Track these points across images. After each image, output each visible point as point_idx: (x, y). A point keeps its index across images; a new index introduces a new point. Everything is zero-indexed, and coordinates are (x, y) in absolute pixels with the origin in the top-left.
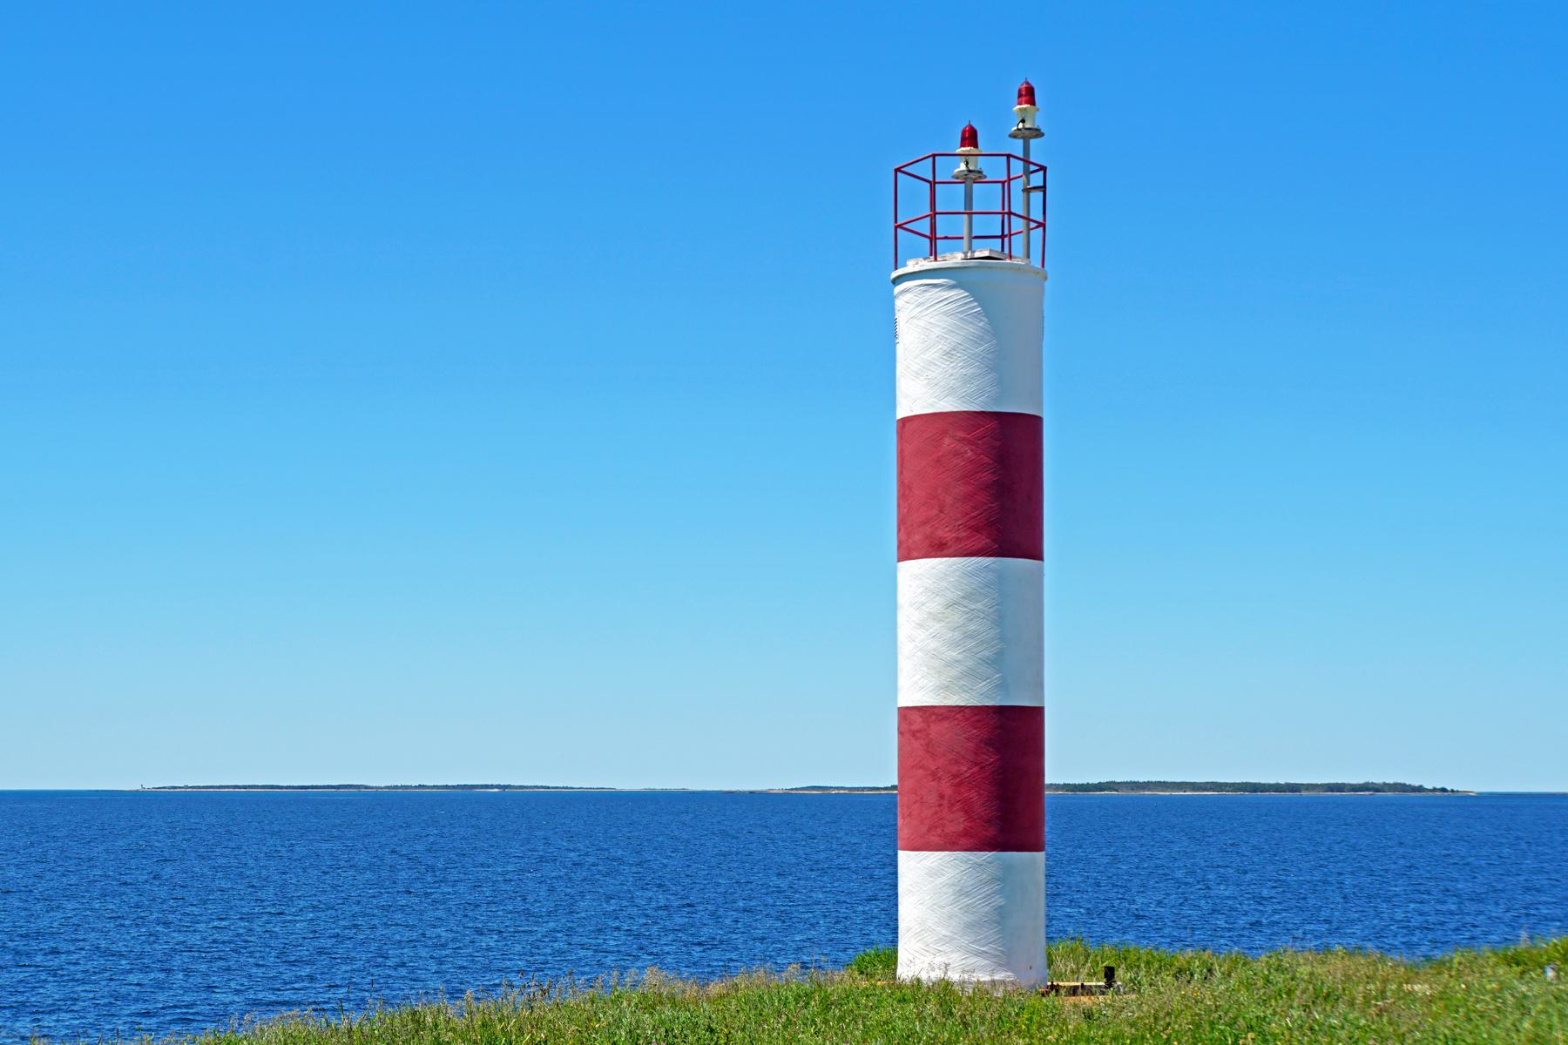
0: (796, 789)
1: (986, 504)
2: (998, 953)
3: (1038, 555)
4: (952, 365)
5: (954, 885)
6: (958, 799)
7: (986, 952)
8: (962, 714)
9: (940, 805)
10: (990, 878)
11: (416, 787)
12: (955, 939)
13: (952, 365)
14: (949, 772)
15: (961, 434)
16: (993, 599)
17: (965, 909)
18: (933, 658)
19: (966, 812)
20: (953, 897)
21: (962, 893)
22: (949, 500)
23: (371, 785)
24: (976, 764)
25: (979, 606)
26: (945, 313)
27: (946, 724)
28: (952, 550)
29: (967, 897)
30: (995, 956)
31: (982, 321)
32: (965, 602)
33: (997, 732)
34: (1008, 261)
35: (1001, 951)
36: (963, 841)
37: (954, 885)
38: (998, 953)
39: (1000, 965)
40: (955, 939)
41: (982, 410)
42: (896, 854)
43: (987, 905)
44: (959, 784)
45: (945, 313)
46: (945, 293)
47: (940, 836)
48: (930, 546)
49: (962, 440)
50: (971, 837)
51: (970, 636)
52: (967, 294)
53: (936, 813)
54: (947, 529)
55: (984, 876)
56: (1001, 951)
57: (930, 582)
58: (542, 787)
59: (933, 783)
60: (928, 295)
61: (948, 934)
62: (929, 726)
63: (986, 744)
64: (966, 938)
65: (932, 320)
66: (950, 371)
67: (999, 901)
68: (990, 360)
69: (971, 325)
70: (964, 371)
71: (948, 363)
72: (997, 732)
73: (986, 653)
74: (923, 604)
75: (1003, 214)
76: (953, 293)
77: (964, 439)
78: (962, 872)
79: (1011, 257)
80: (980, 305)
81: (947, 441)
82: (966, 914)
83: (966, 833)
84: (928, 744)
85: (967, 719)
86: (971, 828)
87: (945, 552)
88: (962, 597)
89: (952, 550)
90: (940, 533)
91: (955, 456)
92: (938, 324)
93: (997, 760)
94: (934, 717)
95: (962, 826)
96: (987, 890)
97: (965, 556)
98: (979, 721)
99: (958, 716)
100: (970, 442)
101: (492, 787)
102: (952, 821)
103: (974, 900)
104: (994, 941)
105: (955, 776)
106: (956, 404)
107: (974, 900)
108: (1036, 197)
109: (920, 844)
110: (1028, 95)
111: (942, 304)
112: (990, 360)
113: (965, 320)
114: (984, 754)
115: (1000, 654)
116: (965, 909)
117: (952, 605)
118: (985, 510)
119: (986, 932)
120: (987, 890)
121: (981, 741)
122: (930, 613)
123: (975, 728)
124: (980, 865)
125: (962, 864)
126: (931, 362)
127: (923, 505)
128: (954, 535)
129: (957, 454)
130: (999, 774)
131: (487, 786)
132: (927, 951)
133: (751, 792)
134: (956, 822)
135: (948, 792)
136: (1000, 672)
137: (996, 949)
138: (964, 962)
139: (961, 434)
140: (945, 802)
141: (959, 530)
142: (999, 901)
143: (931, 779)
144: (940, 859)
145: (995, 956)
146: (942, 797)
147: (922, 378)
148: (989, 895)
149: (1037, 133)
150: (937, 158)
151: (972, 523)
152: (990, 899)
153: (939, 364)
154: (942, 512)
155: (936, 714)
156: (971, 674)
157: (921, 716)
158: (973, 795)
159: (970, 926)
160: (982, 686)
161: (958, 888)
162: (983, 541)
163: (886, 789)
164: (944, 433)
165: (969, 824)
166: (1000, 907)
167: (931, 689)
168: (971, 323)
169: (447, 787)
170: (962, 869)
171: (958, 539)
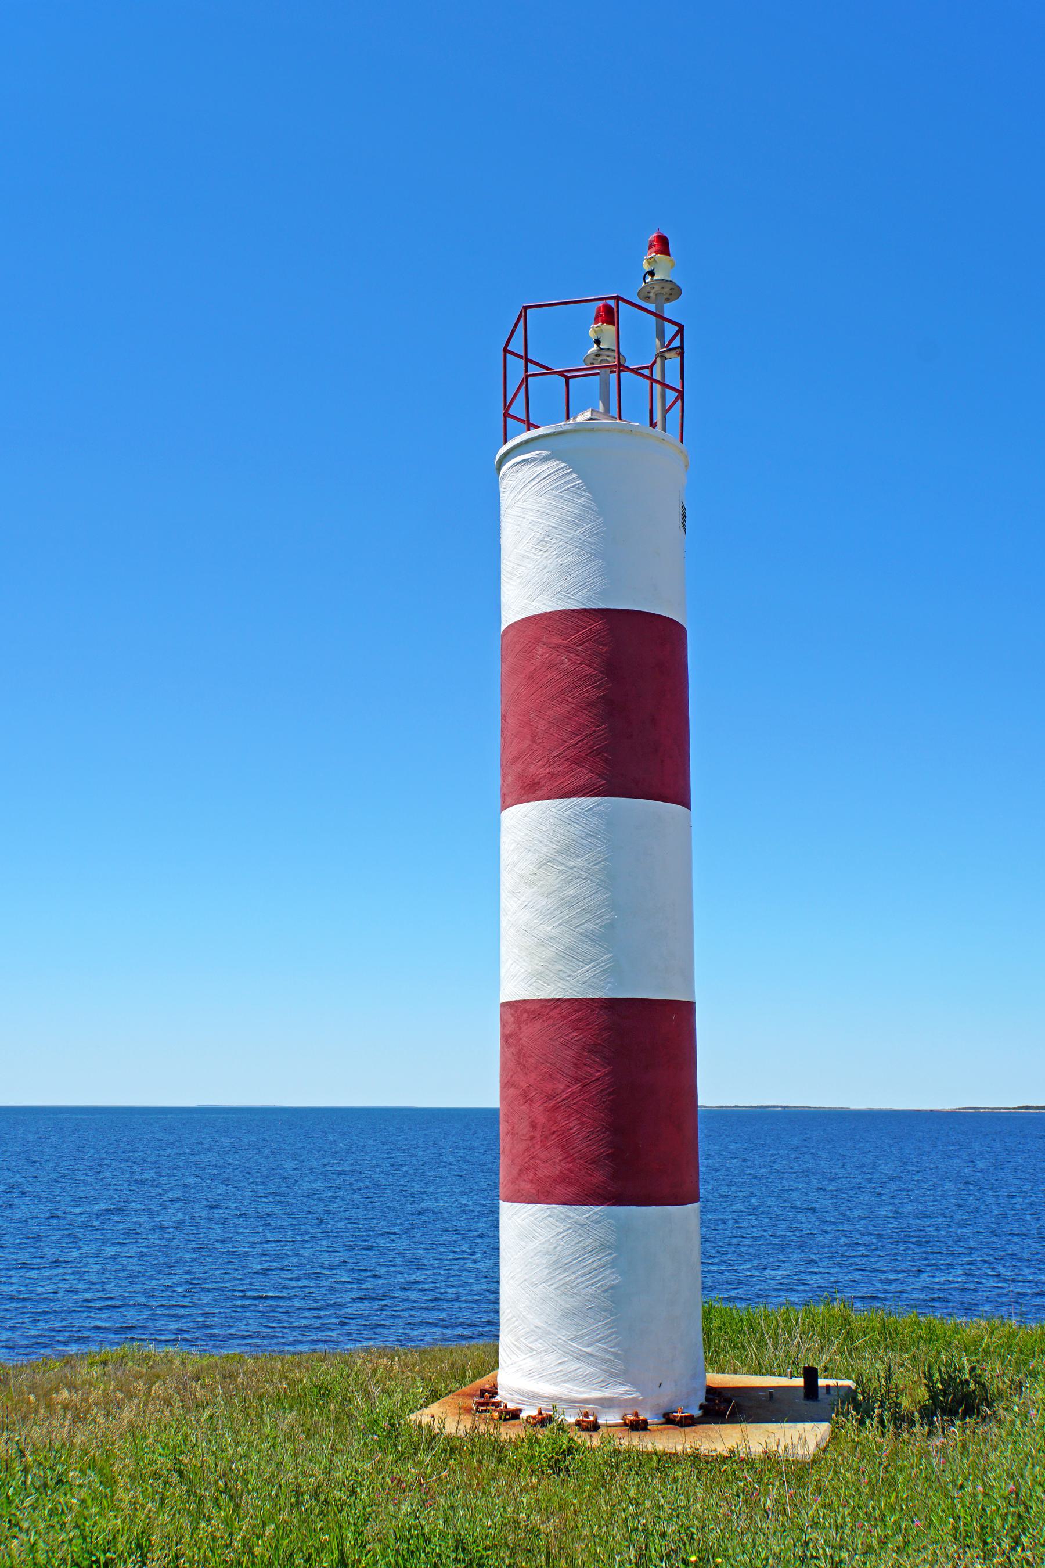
0: (959, 1109)
1: (589, 728)
2: (608, 1356)
3: (685, 801)
4: (546, 555)
5: (547, 1253)
6: (554, 1129)
7: (591, 1355)
8: (558, 1010)
9: (532, 1138)
10: (596, 1244)
11: (733, 1107)
12: (550, 1333)
13: (546, 555)
14: (542, 1092)
15: (557, 640)
16: (600, 852)
17: (562, 1289)
18: (524, 934)
19: (563, 1147)
20: (547, 1271)
21: (559, 1266)
22: (542, 725)
23: (707, 1105)
24: (577, 1080)
25: (580, 862)
26: (537, 493)
27: (538, 1025)
28: (545, 790)
29: (565, 1271)
30: (606, 1361)
31: (581, 496)
32: (561, 859)
33: (606, 1035)
34: (618, 421)
35: (614, 1354)
36: (560, 1190)
37: (547, 1253)
38: (608, 1356)
39: (612, 1375)
40: (550, 1333)
41: (583, 607)
42: (495, 1211)
43: (592, 1284)
44: (555, 1108)
45: (537, 493)
46: (538, 468)
47: (531, 1181)
48: (523, 788)
49: (557, 647)
50: (570, 1184)
51: (568, 903)
52: (563, 465)
53: (527, 1149)
54: (541, 762)
55: (589, 1241)
56: (614, 1354)
57: (521, 834)
58: (807, 1107)
59: (523, 1107)
60: (520, 475)
61: (541, 1324)
62: (520, 1029)
63: (589, 1051)
64: (564, 1332)
65: (525, 505)
66: (544, 563)
67: (612, 1278)
68: (591, 543)
69: (568, 503)
70: (560, 561)
71: (541, 553)
72: (606, 1035)
73: (591, 926)
74: (515, 865)
75: (620, 371)
76: (545, 466)
77: (560, 646)
78: (558, 1234)
79: (620, 419)
80: (580, 477)
81: (540, 650)
82: (563, 1297)
83: (563, 1179)
84: (519, 1052)
85: (565, 1018)
86: (570, 1171)
87: (539, 793)
88: (560, 852)
89: (545, 790)
90: (532, 769)
91: (549, 667)
92: (531, 507)
93: (606, 1075)
94: (525, 1016)
95: (559, 1168)
96: (593, 1261)
97: (557, 798)
98: (579, 1020)
99: (552, 1013)
100: (568, 650)
101: (777, 1107)
102: (546, 1162)
103: (575, 1276)
104: (602, 1338)
105: (550, 1097)
106: (550, 603)
107: (575, 1276)
108: (673, 361)
109: (519, 1197)
110: (663, 245)
111: (534, 482)
112: (591, 543)
113: (561, 497)
114: (588, 1065)
115: (611, 926)
116: (562, 1289)
117: (545, 863)
118: (587, 736)
119: (591, 1325)
120: (593, 1261)
121: (584, 1048)
122: (521, 876)
123: (575, 1030)
124: (583, 1225)
125: (558, 1224)
126: (524, 556)
127: (515, 736)
128: (547, 771)
129: (551, 666)
130: (610, 1094)
131: (774, 1107)
132: (518, 1348)
133: (931, 1111)
134: (552, 1164)
135: (542, 1120)
136: (610, 952)
137: (605, 1350)
138: (560, 1368)
139: (557, 640)
140: (538, 1134)
141: (554, 763)
142: (612, 1278)
143: (522, 1102)
144: (532, 1215)
145: (606, 1361)
146: (534, 1126)
147: (515, 578)
148: (595, 1270)
149: (674, 292)
150: (529, 311)
151: (571, 752)
152: (598, 1275)
153: (532, 556)
154: (534, 742)
155: (528, 1012)
156: (570, 954)
157: (513, 1015)
158: (573, 1123)
159: (569, 1314)
160: (584, 972)
161: (554, 1258)
162: (585, 776)
163: (1014, 1109)
164: (537, 641)
165: (567, 1166)
166: (612, 1287)
167: (523, 976)
168: (568, 500)
169: (751, 1107)
170: (559, 1230)
171: (553, 776)
